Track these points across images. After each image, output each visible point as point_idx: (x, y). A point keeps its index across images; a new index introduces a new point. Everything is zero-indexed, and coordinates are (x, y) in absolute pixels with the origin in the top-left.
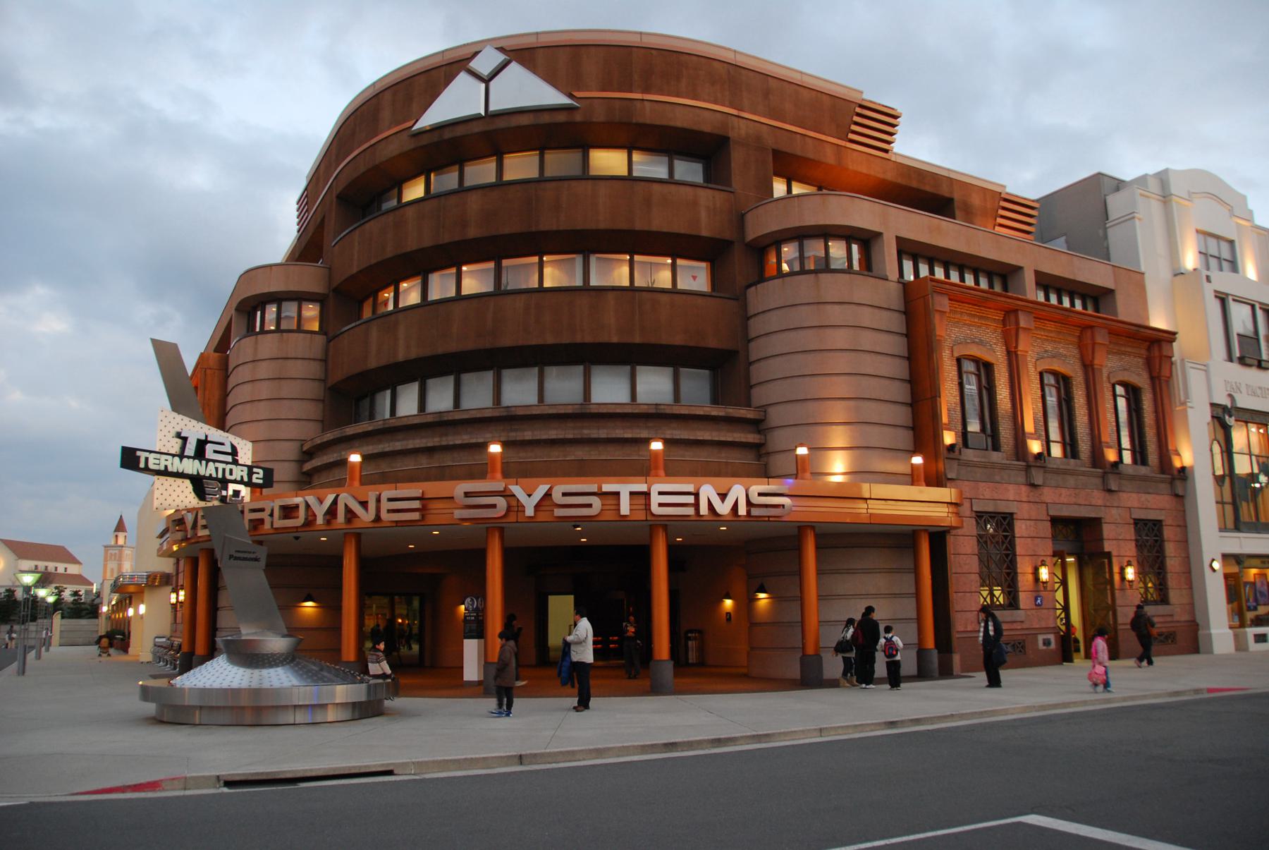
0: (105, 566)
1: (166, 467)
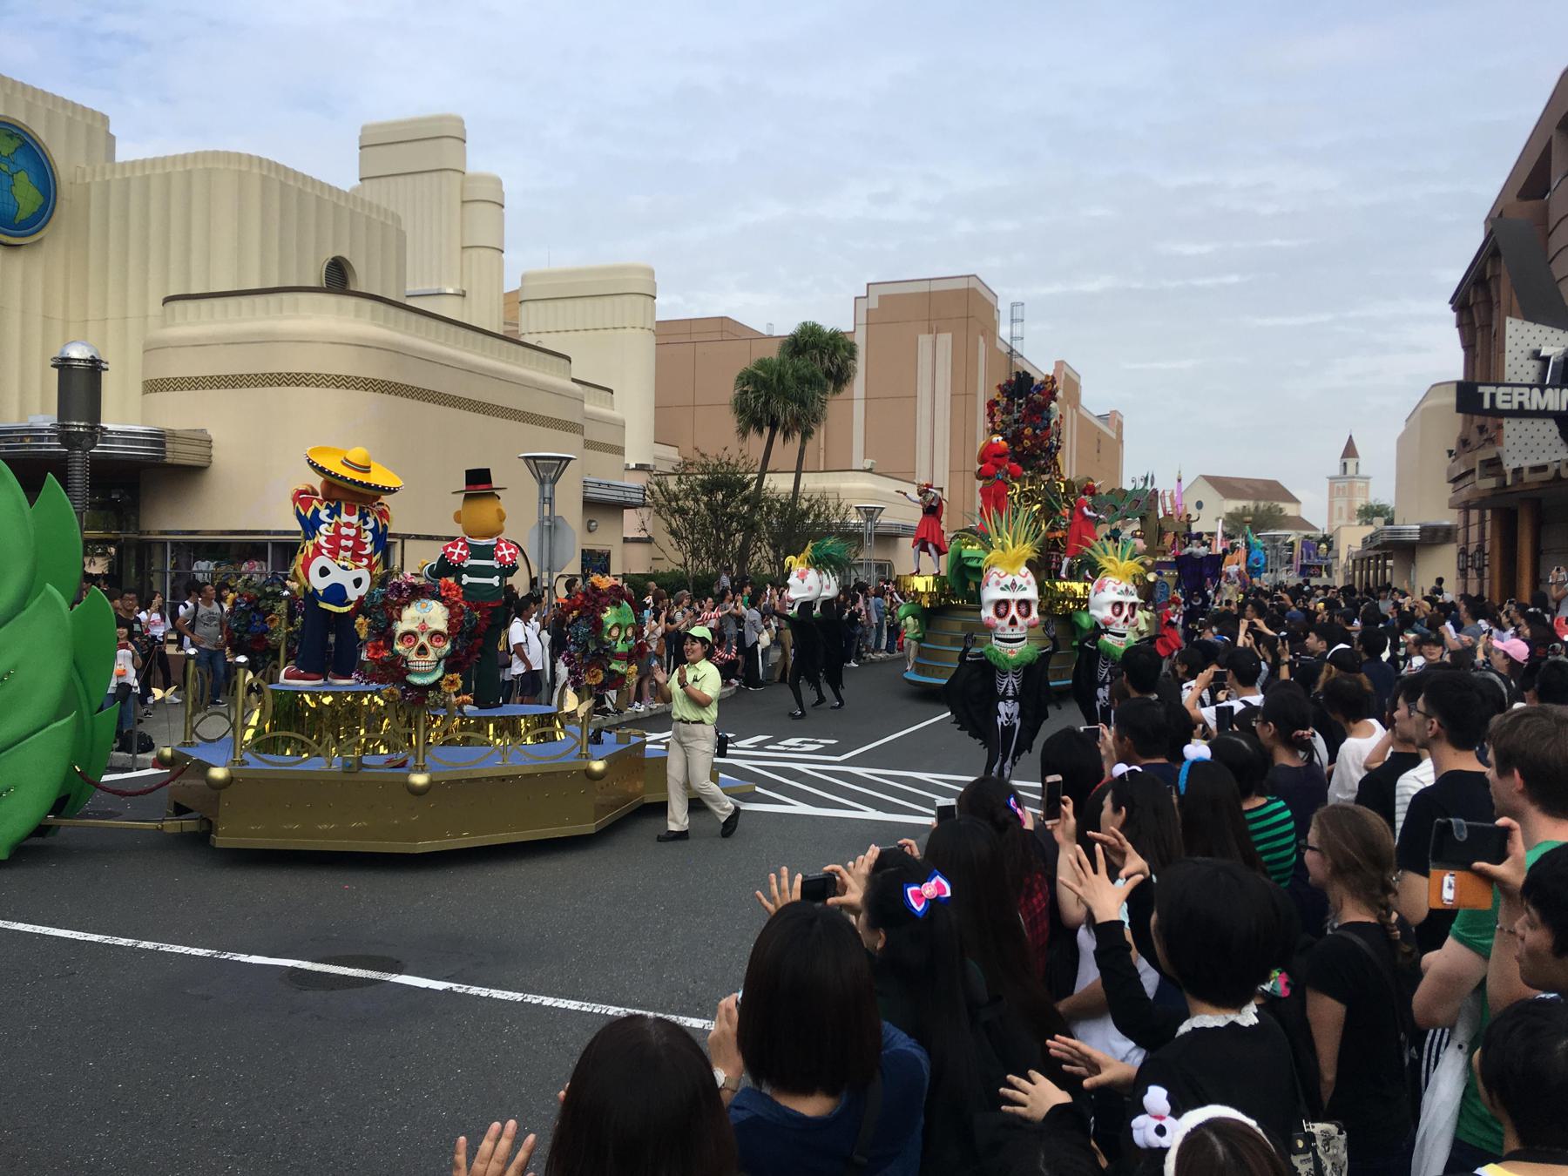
0: (1331, 504)
1: (1521, 404)
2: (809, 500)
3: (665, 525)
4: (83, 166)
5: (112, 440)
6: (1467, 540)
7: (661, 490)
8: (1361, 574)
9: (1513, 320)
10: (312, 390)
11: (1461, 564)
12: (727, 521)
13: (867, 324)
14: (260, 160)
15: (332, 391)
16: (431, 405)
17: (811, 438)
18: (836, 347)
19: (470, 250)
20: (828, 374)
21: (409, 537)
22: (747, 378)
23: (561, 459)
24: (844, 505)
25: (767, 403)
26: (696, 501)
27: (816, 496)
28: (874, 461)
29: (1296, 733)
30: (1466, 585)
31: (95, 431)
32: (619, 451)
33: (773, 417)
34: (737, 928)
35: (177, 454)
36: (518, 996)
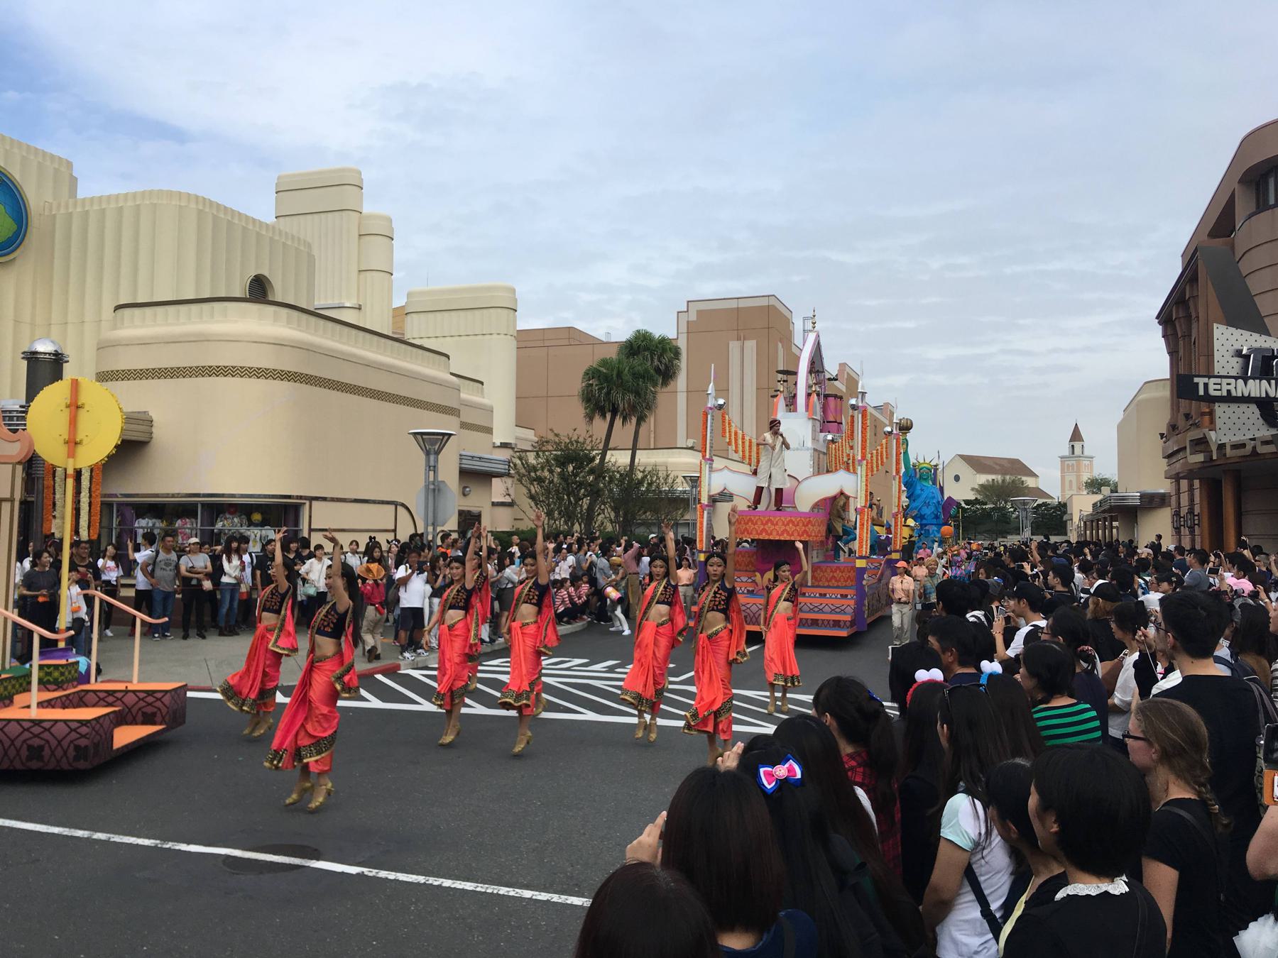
0: (1063, 478)
1: (1229, 391)
2: (643, 472)
3: (525, 491)
4: (50, 201)
6: (1179, 504)
7: (522, 463)
8: (1092, 533)
9: (1219, 326)
10: (237, 380)
11: (1175, 524)
12: (576, 488)
13: (688, 333)
14: (197, 197)
15: (254, 380)
16: (335, 392)
17: (645, 421)
18: (664, 350)
20: (658, 370)
21: (317, 499)
22: (592, 374)
23: (443, 434)
24: (672, 476)
25: (608, 393)
26: (551, 472)
27: (649, 469)
28: (695, 441)
30: (1180, 541)
32: (489, 430)
33: (613, 405)
34: (605, 820)
36: (421, 879)
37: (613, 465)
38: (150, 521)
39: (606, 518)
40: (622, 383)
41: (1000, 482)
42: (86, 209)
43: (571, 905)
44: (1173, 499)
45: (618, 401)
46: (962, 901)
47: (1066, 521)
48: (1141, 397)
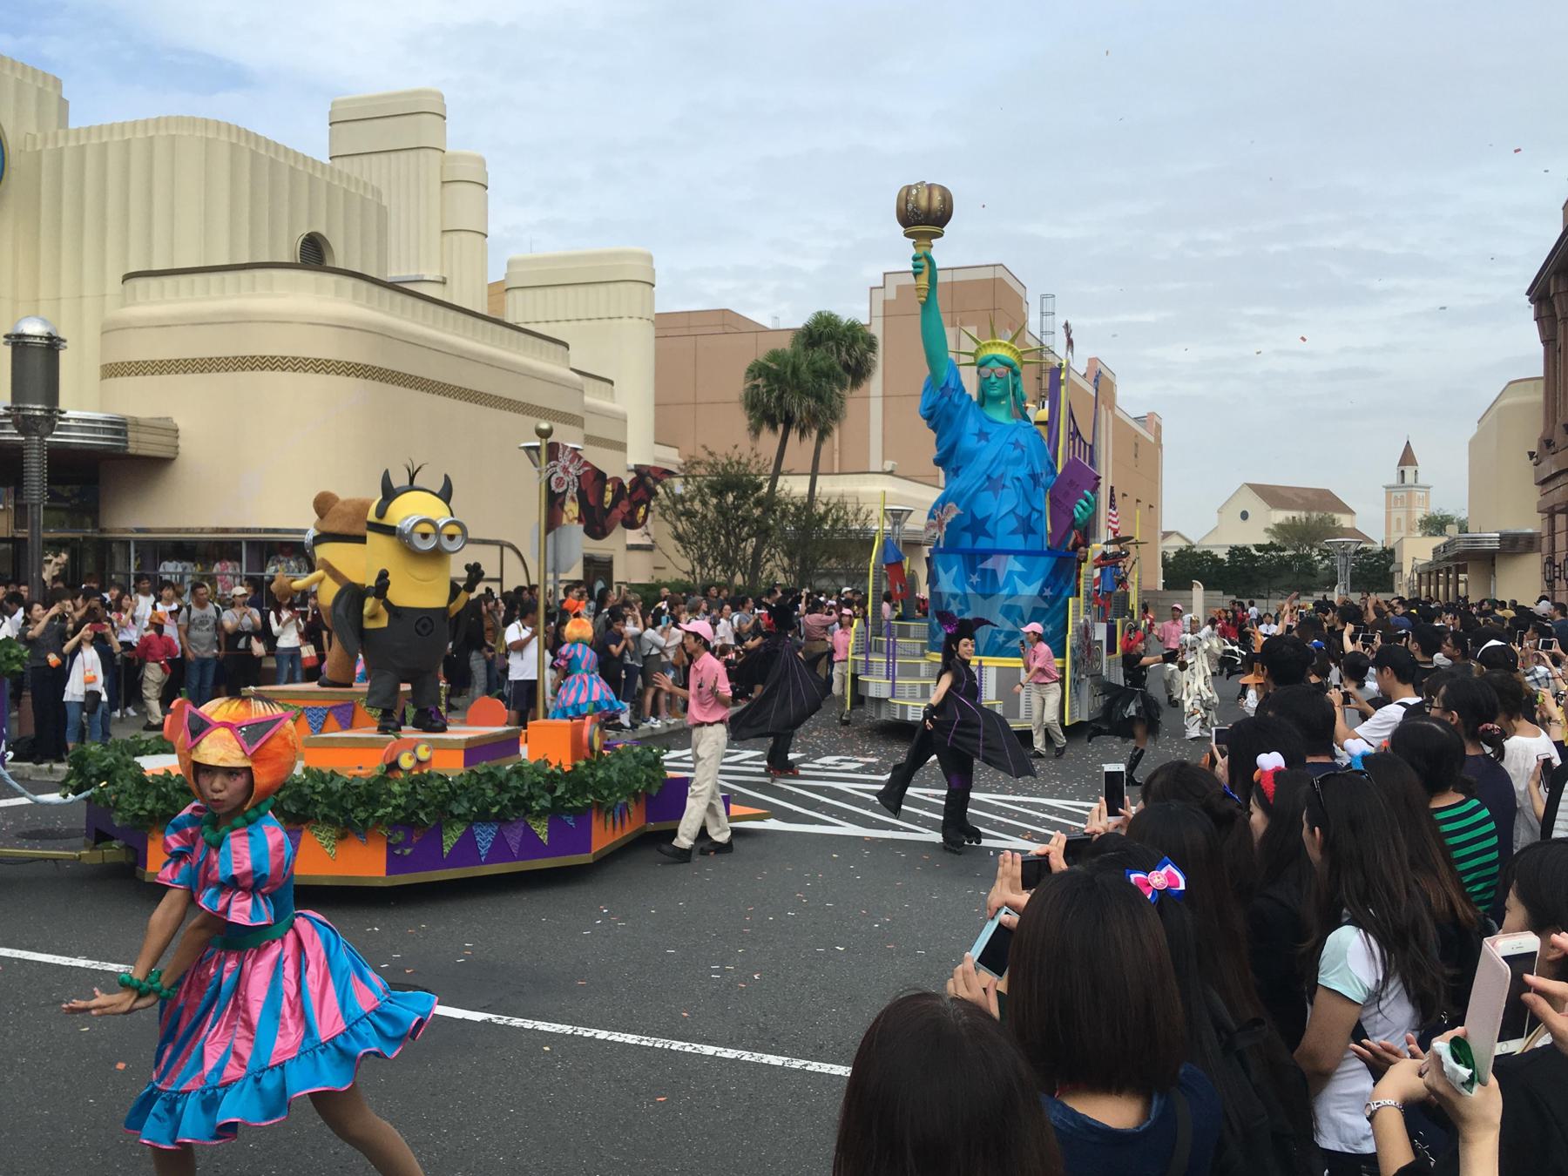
0: (1388, 515)
2: (827, 504)
3: (668, 528)
5: (68, 428)
6: (1554, 548)
7: (666, 492)
10: (289, 375)
11: (1548, 574)
18: (855, 340)
19: (450, 234)
20: (847, 367)
22: (757, 370)
24: (864, 510)
26: (704, 503)
27: (834, 500)
29: (1484, 726)
31: (53, 414)
32: (621, 447)
35: (139, 445)
36: (568, 1029)
37: (788, 495)
38: (179, 565)
39: (777, 566)
40: (798, 383)
41: (1304, 520)
42: (81, 143)
43: (768, 1065)
44: (1545, 543)
45: (793, 408)
46: (1345, 1069)
47: (1393, 573)
48: (1504, 402)
